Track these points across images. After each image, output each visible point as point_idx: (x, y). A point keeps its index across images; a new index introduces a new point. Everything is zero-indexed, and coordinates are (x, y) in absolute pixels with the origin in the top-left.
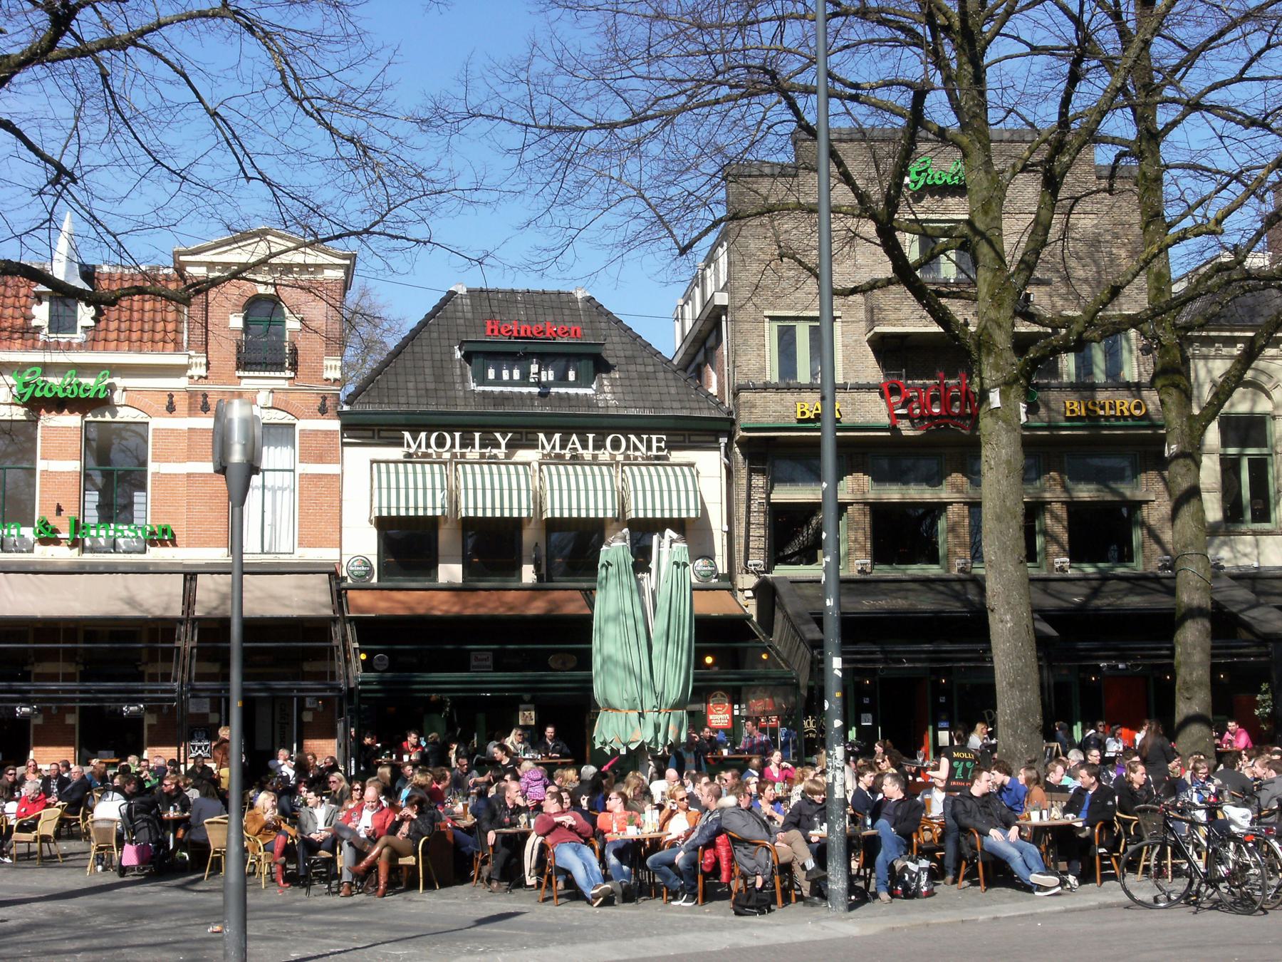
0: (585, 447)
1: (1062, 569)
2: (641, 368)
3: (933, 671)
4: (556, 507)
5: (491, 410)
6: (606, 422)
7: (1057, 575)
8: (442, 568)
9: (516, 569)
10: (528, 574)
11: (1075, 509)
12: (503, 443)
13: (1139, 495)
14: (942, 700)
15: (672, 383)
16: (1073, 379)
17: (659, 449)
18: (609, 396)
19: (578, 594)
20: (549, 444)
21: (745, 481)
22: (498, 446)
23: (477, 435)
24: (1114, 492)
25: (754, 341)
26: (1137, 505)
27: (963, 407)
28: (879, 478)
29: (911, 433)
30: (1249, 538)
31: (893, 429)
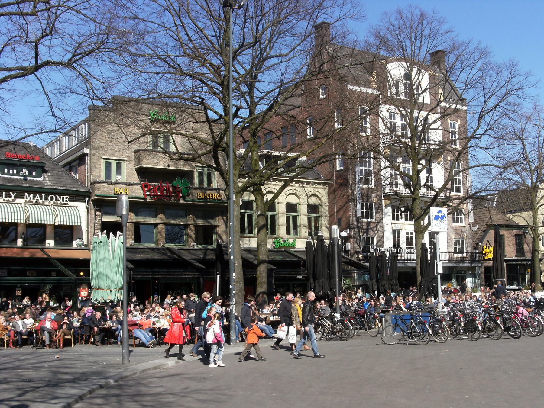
0: (41, 199)
1: (193, 246)
2: (57, 172)
3: (153, 278)
4: (32, 220)
5: (8, 184)
6: (49, 191)
7: (191, 248)
8: (47, 242)
9: (15, 240)
10: (20, 242)
11: (196, 226)
12: (13, 196)
13: (216, 224)
14: (156, 288)
15: (68, 178)
16: (198, 186)
17: (66, 201)
18: (48, 182)
19: (39, 250)
20: (29, 197)
21: (94, 214)
22: (10, 197)
23: (4, 193)
24: (208, 222)
25: (98, 166)
26: (216, 227)
27: (167, 193)
28: (137, 215)
29: (150, 200)
30: (247, 238)
31: (145, 199)
